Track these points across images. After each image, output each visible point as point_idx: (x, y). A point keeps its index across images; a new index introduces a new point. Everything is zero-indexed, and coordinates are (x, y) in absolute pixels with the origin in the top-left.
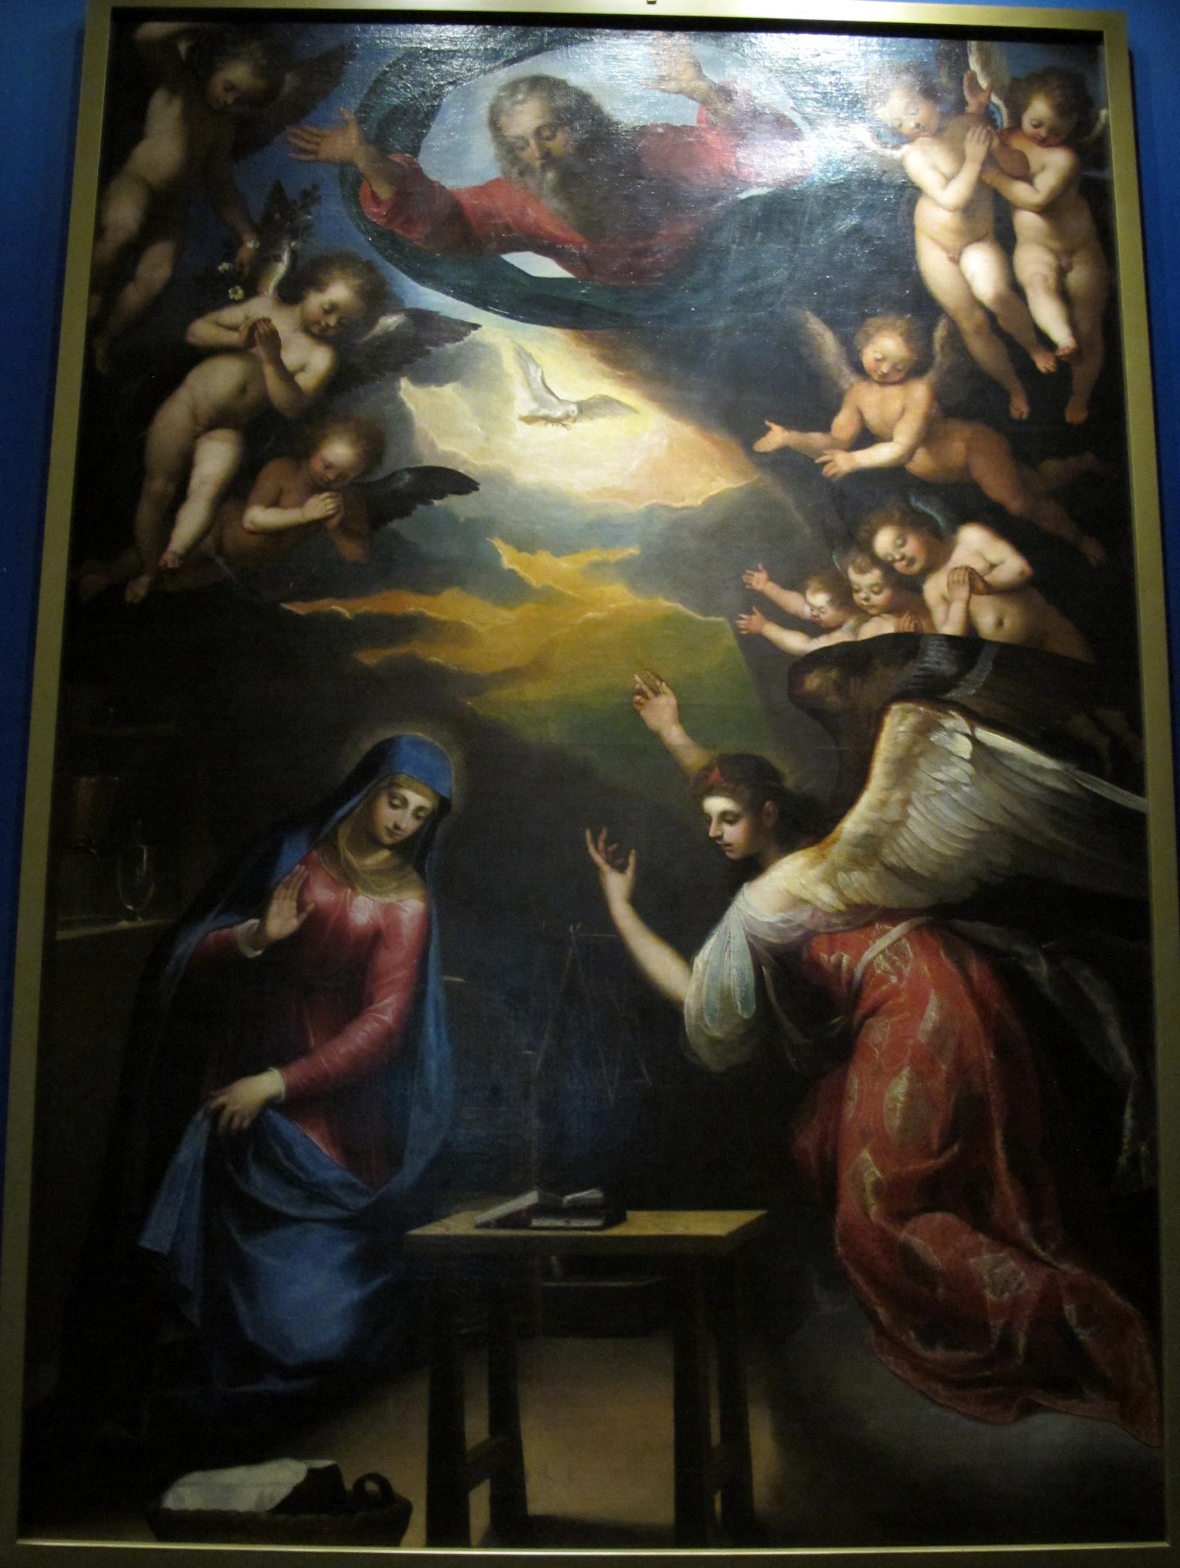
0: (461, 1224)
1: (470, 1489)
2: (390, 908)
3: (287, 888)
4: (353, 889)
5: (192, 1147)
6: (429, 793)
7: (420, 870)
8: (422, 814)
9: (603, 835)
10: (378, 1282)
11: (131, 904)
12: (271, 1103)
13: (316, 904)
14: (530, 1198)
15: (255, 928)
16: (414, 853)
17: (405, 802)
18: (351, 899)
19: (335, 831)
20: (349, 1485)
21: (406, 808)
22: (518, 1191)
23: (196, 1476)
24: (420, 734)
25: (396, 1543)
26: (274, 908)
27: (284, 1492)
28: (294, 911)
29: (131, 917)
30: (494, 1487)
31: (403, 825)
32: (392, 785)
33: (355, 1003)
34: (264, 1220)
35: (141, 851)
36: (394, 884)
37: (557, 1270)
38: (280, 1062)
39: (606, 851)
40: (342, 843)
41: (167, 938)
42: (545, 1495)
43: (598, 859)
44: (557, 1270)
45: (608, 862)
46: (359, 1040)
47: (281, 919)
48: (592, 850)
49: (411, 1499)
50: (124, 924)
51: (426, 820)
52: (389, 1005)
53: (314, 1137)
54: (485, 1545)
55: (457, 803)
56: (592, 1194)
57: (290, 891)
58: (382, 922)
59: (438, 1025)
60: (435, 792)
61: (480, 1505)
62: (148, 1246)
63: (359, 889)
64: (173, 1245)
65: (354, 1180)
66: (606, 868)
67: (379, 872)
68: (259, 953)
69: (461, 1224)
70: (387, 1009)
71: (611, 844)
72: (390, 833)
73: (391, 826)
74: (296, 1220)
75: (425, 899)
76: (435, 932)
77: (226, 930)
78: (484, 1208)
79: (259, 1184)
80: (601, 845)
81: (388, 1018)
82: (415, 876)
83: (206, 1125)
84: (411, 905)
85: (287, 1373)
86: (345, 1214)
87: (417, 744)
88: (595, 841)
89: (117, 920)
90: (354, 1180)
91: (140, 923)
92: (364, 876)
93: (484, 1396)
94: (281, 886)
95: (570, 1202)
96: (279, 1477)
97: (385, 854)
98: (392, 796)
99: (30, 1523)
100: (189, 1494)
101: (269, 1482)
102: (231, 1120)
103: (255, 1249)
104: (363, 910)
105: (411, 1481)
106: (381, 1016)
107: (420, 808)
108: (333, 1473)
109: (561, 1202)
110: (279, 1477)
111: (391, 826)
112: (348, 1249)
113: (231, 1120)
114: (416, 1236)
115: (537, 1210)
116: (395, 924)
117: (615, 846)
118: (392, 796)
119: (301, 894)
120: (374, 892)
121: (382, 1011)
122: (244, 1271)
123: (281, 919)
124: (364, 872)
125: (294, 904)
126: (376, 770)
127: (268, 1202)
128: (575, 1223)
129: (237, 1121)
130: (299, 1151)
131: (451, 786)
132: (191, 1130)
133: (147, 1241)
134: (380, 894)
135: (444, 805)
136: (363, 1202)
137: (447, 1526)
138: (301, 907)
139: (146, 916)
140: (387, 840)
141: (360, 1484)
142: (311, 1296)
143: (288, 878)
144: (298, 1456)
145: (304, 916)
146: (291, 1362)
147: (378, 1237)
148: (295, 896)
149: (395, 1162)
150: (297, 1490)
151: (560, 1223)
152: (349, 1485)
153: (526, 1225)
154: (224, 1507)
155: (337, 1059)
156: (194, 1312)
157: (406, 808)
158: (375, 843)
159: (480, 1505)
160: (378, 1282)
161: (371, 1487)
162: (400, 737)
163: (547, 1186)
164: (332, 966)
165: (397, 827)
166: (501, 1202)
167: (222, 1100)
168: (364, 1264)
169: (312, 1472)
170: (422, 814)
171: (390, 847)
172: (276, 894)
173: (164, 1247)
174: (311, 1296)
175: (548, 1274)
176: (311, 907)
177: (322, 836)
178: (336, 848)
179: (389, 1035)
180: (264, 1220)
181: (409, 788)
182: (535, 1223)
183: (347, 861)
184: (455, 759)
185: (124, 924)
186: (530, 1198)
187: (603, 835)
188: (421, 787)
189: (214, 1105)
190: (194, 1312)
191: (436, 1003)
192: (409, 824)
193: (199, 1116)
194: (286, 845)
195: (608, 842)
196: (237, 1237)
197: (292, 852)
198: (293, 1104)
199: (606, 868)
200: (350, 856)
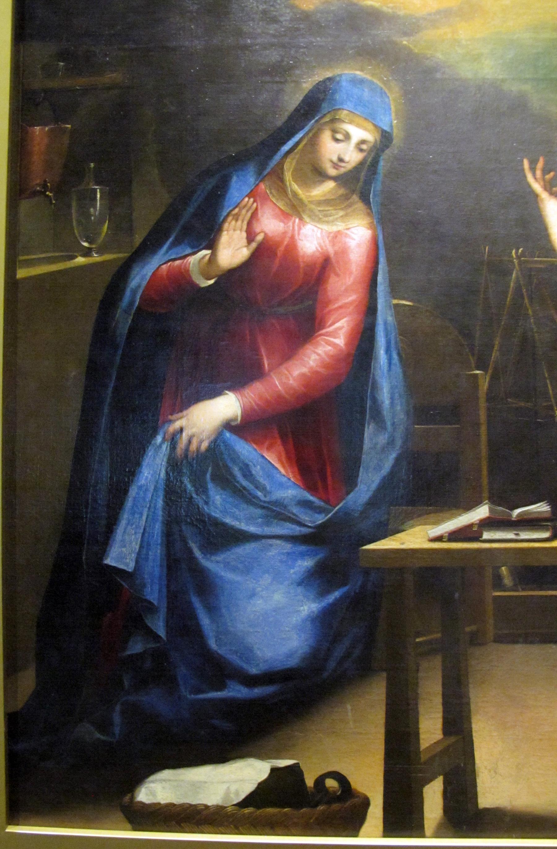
0: (416, 537)
1: (423, 786)
2: (336, 235)
3: (237, 220)
4: (301, 219)
5: (152, 469)
6: (371, 127)
7: (365, 199)
8: (364, 147)
9: (540, 165)
10: (336, 594)
11: (86, 241)
12: (229, 426)
13: (266, 234)
14: (483, 512)
15: (207, 257)
16: (359, 184)
17: (347, 137)
18: (300, 229)
19: (281, 164)
20: (310, 782)
21: (346, 143)
22: (469, 507)
23: (166, 774)
24: (358, 73)
25: (355, 833)
26: (224, 238)
27: (248, 788)
28: (244, 241)
29: (87, 253)
30: (446, 783)
31: (347, 158)
32: (333, 121)
33: (307, 326)
34: (224, 538)
35: (95, 190)
36: (341, 213)
37: (508, 581)
38: (237, 384)
39: (544, 180)
40: (288, 176)
41: (123, 272)
42: (492, 791)
43: (537, 187)
44: (508, 581)
45: (545, 189)
46: (312, 363)
47: (232, 249)
48: (530, 178)
49: (369, 795)
50: (80, 260)
51: (370, 151)
52: (340, 328)
53: (271, 457)
54: (437, 835)
55: (397, 134)
56: (542, 508)
57: (239, 222)
58: (331, 251)
59: (388, 350)
60: (376, 126)
61: (433, 799)
62: (113, 564)
63: (305, 217)
64: (137, 562)
65: (311, 498)
66: (544, 195)
67: (327, 202)
68: (212, 282)
69: (416, 537)
70: (336, 335)
71: (549, 172)
72: (335, 166)
73: (335, 159)
74: (255, 538)
75: (371, 226)
76: (382, 260)
77: (178, 262)
78: (437, 523)
79: (218, 504)
80: (539, 173)
81: (340, 341)
82: (360, 205)
83: (165, 447)
84: (357, 234)
85: (251, 681)
86: (304, 530)
87: (357, 82)
88: (533, 170)
89: (73, 257)
90: (311, 498)
91: (96, 258)
92: (313, 206)
93: (438, 700)
94: (230, 218)
95: (519, 515)
96: (244, 775)
97: (330, 185)
98: (334, 131)
99: (15, 813)
100: (160, 789)
101: (236, 779)
102: (190, 442)
103: (213, 564)
104: (311, 239)
105: (369, 780)
106: (332, 339)
107: (363, 142)
108: (295, 771)
109: (511, 515)
110: (244, 775)
111: (335, 159)
112: (307, 563)
113: (190, 442)
114: (374, 551)
115: (488, 523)
116: (343, 252)
117: (552, 174)
118: (334, 131)
119: (249, 224)
120: (320, 221)
121: (333, 334)
122: (205, 585)
123: (232, 249)
124: (311, 202)
125: (244, 235)
126: (315, 107)
127: (228, 520)
128: (524, 535)
129: (193, 447)
130: (257, 471)
131: (391, 120)
132: (150, 452)
133: (109, 561)
134: (328, 222)
135: (386, 138)
136: (321, 519)
137: (402, 817)
138: (250, 238)
139: (100, 251)
140: (332, 172)
141: (320, 781)
142: (271, 610)
143: (237, 210)
144: (261, 756)
145: (254, 245)
146: (254, 671)
147: (335, 552)
148: (245, 227)
149: (350, 481)
150: (262, 786)
151: (510, 535)
152: (310, 782)
153: (477, 538)
154: (194, 801)
155: (291, 382)
156: (159, 626)
157: (346, 143)
158: (320, 175)
159: (433, 799)
160: (336, 594)
161: (331, 783)
162: (340, 76)
163: (496, 499)
164: (284, 292)
165: (341, 160)
166: (449, 519)
167: (177, 425)
168: (323, 577)
169: (274, 770)
170: (364, 147)
171: (335, 179)
172: (226, 226)
173: (130, 567)
174: (271, 610)
175: (498, 583)
176: (260, 238)
177: (268, 170)
178: (282, 180)
179: (338, 359)
180: (224, 538)
181: (351, 122)
182: (486, 535)
183: (295, 194)
184: (393, 97)
185: (80, 260)
186: (483, 512)
187: (540, 165)
188: (361, 121)
189: (177, 425)
190: (159, 626)
191: (385, 323)
192: (353, 157)
193: (159, 439)
194: (234, 178)
195: (545, 171)
196: (197, 553)
197: (240, 187)
198: (246, 427)
199: (544, 195)
200: (295, 187)
